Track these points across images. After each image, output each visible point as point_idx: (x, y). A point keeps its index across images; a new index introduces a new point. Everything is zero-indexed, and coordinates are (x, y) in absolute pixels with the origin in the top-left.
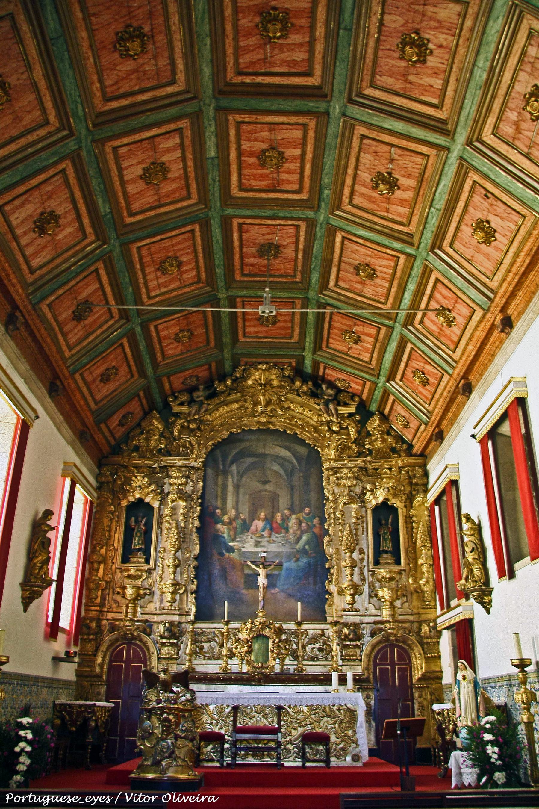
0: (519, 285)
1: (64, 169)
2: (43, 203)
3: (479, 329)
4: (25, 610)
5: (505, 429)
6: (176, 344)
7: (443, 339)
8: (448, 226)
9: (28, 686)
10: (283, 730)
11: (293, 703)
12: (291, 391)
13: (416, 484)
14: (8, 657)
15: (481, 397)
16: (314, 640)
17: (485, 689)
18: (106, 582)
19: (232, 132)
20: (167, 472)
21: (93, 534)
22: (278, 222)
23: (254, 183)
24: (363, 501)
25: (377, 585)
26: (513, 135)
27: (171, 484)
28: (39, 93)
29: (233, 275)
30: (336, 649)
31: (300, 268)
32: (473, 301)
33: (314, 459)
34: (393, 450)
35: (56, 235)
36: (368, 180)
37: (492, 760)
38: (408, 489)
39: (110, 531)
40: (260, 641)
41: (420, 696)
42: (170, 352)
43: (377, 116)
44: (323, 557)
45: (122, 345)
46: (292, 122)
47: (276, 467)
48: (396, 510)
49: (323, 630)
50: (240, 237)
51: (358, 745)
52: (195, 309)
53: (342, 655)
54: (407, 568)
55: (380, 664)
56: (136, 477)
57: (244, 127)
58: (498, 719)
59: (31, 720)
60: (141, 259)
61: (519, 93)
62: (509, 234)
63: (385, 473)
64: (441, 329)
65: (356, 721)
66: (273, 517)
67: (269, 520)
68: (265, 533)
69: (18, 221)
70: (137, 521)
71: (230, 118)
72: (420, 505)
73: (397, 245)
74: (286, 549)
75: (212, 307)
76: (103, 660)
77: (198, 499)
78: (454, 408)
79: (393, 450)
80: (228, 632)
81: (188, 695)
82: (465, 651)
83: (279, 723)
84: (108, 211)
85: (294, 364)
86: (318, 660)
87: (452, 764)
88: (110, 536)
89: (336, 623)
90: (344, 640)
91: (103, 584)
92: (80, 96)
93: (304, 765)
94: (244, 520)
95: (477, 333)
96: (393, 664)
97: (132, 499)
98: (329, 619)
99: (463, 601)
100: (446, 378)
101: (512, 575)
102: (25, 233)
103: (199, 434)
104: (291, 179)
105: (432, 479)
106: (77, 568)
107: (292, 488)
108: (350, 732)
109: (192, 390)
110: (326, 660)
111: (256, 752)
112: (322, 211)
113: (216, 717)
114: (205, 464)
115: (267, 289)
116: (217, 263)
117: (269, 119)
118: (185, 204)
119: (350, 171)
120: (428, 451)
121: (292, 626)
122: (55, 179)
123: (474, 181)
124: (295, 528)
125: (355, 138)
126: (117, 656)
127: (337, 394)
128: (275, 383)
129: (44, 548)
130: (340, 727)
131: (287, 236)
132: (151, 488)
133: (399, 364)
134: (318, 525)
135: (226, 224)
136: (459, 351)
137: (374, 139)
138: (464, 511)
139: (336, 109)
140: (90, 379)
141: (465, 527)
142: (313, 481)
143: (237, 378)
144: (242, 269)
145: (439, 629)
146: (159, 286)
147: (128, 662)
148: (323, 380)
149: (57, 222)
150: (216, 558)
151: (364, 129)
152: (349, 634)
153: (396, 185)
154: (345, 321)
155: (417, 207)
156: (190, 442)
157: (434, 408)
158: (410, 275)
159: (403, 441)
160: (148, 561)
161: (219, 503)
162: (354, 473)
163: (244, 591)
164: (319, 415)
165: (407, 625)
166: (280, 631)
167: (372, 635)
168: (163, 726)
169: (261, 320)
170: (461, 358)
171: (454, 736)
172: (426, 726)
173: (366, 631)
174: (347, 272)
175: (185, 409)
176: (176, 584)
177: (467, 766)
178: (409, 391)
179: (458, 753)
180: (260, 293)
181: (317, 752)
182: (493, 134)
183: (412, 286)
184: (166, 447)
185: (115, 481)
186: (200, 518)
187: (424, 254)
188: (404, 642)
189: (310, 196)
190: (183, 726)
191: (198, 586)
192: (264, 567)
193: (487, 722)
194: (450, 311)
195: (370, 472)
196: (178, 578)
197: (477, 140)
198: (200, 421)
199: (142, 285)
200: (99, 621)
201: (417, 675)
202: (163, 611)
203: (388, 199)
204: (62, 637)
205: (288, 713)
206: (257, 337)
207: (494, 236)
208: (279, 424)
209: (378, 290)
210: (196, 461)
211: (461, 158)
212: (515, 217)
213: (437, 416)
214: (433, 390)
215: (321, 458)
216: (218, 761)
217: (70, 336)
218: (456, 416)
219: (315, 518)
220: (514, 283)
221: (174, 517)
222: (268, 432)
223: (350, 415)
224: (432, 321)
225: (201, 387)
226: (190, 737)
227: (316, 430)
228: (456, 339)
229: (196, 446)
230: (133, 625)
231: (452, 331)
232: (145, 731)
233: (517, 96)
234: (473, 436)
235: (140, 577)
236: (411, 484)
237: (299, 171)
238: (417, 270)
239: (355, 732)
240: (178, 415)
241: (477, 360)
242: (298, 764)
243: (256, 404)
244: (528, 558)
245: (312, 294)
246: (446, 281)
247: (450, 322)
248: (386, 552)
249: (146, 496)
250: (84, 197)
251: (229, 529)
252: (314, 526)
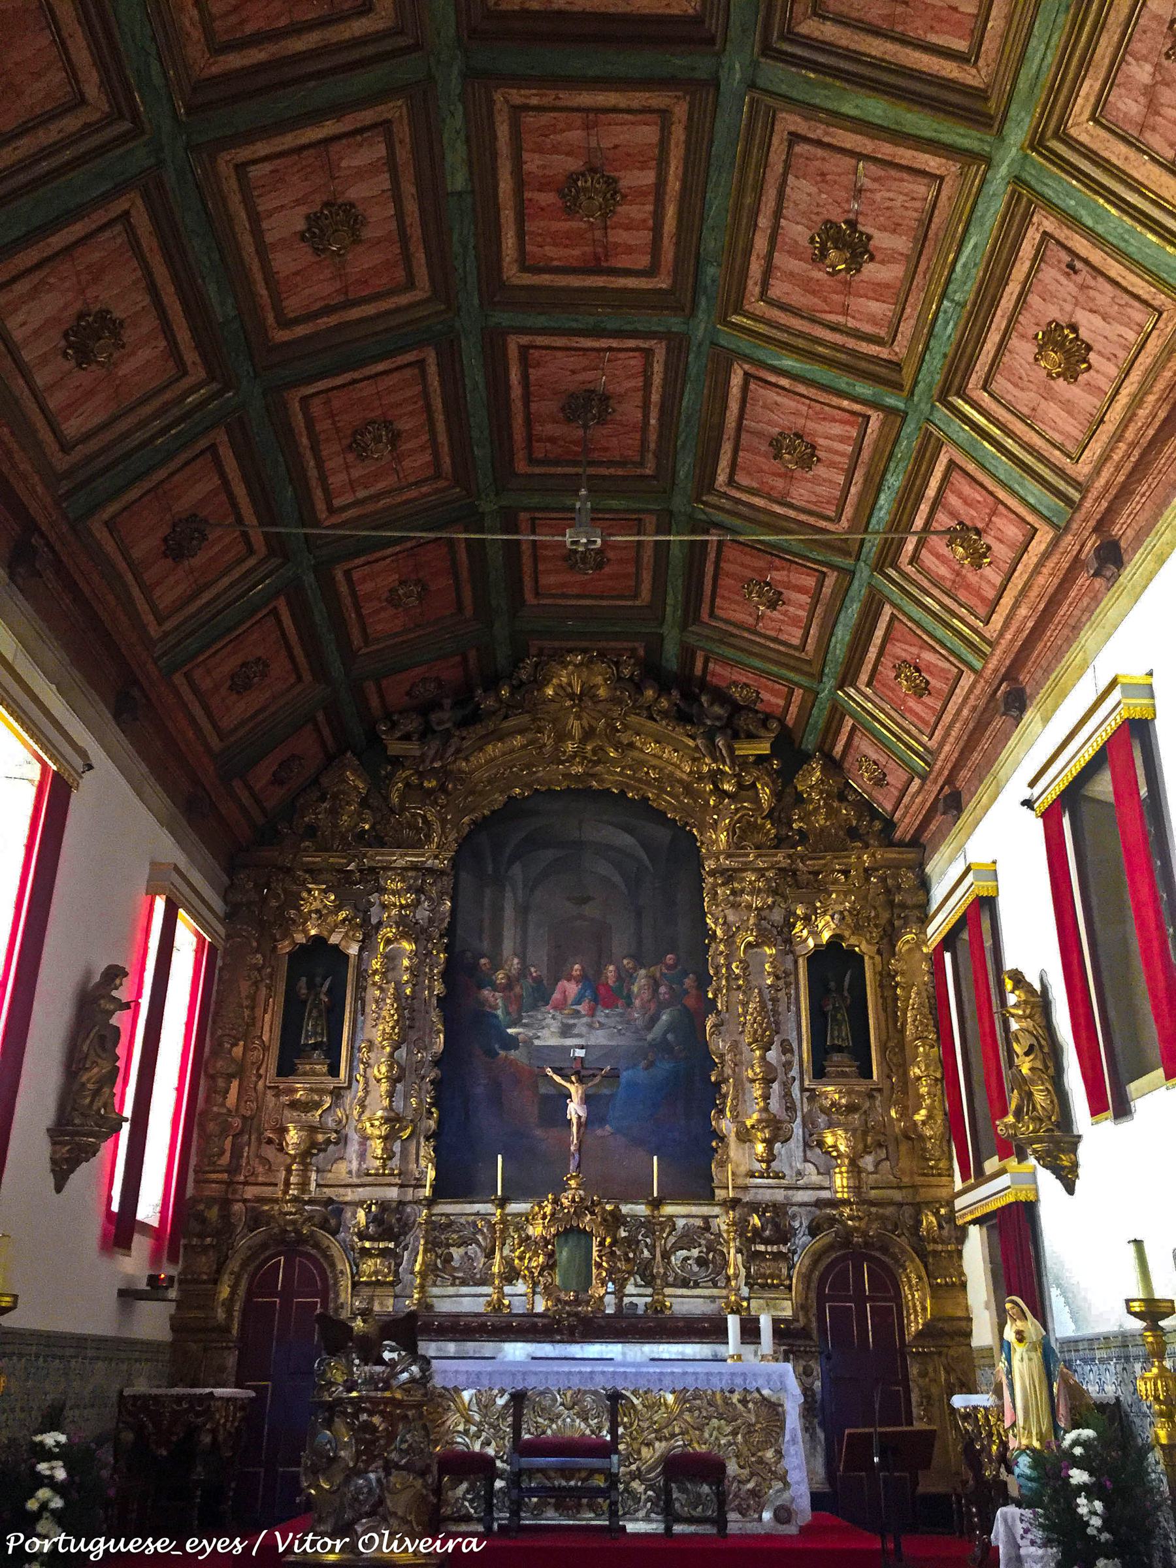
0: (1140, 470)
1: (127, 213)
2: (83, 292)
3: (1045, 571)
4: (59, 1189)
5: (1103, 787)
6: (392, 611)
7: (962, 595)
8: (980, 341)
9: (61, 1358)
10: (621, 1447)
11: (643, 1385)
12: (636, 709)
13: (903, 906)
14: (16, 1297)
15: (1046, 720)
16: (687, 1239)
17: (1069, 1364)
18: (244, 1117)
19: (503, 131)
20: (377, 880)
21: (216, 1014)
22: (604, 343)
23: (550, 251)
24: (789, 941)
25: (822, 1120)
26: (1139, 119)
27: (384, 907)
28: (59, 30)
29: (512, 460)
30: (735, 1258)
31: (653, 446)
32: (1034, 510)
33: (683, 853)
34: (853, 833)
35: (115, 365)
36: (804, 241)
37: (1090, 1531)
38: (886, 915)
39: (252, 1008)
40: (572, 1240)
41: (923, 1374)
42: (379, 627)
43: (826, 86)
44: (705, 1059)
45: (275, 612)
46: (635, 104)
47: (604, 868)
48: (860, 958)
49: (706, 1219)
50: (525, 377)
51: (787, 1485)
52: (432, 535)
53: (748, 1276)
54: (886, 1086)
55: (831, 1298)
56: (309, 891)
57: (529, 119)
58: (1100, 1437)
59: (63, 1438)
60: (310, 423)
61: (1157, 18)
62: (1122, 354)
63: (836, 881)
64: (958, 574)
65: (783, 1428)
66: (599, 972)
68: (582, 1008)
69: (28, 330)
70: (311, 986)
71: (498, 96)
72: (910, 950)
73: (864, 389)
74: (624, 1042)
75: (466, 531)
76: (233, 1293)
77: (442, 936)
78: (985, 744)
79: (853, 833)
80: (503, 1221)
81: (415, 1369)
82: (1021, 1269)
83: (613, 1431)
84: (233, 313)
85: (641, 652)
86: (697, 1285)
87: (999, 1527)
88: (254, 1018)
89: (734, 1203)
90: (752, 1241)
91: (237, 1122)
92: (154, 38)
93: (668, 1529)
94: (538, 980)
95: (1041, 580)
96: (861, 1300)
97: (300, 938)
98: (720, 1194)
99: (1012, 1162)
100: (967, 680)
101: (1123, 1111)
102: (44, 360)
103: (442, 799)
104: (632, 242)
105: (938, 892)
106: (180, 1090)
107: (639, 915)
108: (770, 1454)
109: (426, 709)
110: (715, 1286)
111: (564, 1499)
112: (701, 315)
113: (477, 1418)
114: (455, 862)
115: (583, 492)
116: (475, 434)
117: (586, 99)
118: (403, 300)
119: (764, 222)
120: (927, 834)
121: (642, 1209)
122: (107, 234)
123: (1045, 233)
124: (646, 996)
125: (775, 141)
126: (262, 1283)
127: (731, 717)
128: (602, 692)
129: (104, 1049)
130: (745, 1441)
131: (626, 372)
132: (342, 915)
133: (865, 651)
134: (693, 992)
135: (493, 345)
136: (998, 620)
137: (819, 143)
138: (1009, 964)
139: (735, 72)
140: (207, 684)
141: (1012, 999)
143: (522, 684)
144: (529, 448)
145: (960, 1222)
146: (352, 485)
147: (287, 1294)
148: (703, 685)
149: (116, 334)
151: (798, 119)
152: (763, 1228)
153: (867, 251)
154: (747, 560)
155: (911, 300)
156: (424, 817)
157: (941, 744)
158: (891, 454)
159: (874, 814)
160: (334, 1071)
161: (486, 945)
162: (768, 880)
163: (538, 1132)
164: (694, 760)
165: (889, 1211)
166: (615, 1220)
167: (813, 1231)
168: (359, 1441)
169: (571, 558)
170: (1001, 635)
171: (1002, 1470)
172: (937, 1444)
173: (800, 1223)
174: (755, 451)
175: (413, 748)
176: (393, 1120)
177: (1033, 1543)
178: (887, 707)
179: (1011, 1510)
180: (569, 503)
181: (698, 1500)
182: (1093, 118)
183: (895, 481)
184: (372, 827)
185: (264, 900)
186: (445, 976)
187: (925, 407)
188: (885, 1249)
189: (675, 282)
190: (403, 1441)
191: (440, 1123)
192: (581, 1081)
193: (1076, 1443)
194: (978, 532)
195: (804, 878)
196: (399, 1104)
197: (1056, 135)
198: (445, 774)
199: (314, 483)
200: (225, 1204)
201: (915, 1325)
202: (367, 1178)
203: (847, 284)
204: (141, 1245)
205: (633, 1406)
206: (565, 596)
207: (1085, 361)
208: (612, 778)
209: (821, 490)
210: (436, 857)
211: (1018, 180)
212: (1138, 314)
213: (946, 760)
214: (938, 705)
215: (698, 850)
216: (479, 1520)
217: (157, 593)
218: (990, 760)
219: (686, 975)
220: (1129, 466)
221: (390, 975)
222: (589, 793)
223: (760, 759)
224: (938, 556)
225: (447, 702)
226: (419, 1465)
227: (688, 790)
228: (990, 594)
229: (437, 826)
230: (300, 1211)
231: (982, 577)
232: (319, 1453)
233: (1154, 25)
234: (1028, 803)
235: (318, 1105)
236: (891, 904)
237: (651, 222)
238: (908, 444)
239: (779, 1453)
240: (397, 762)
241: (1040, 639)
242: (653, 1527)
243: (562, 736)
244: (1160, 1072)
245: (678, 503)
246: (971, 467)
247: (978, 557)
248: (840, 1049)
249: (332, 932)
250: (176, 279)
251: (504, 999)
252: (686, 992)
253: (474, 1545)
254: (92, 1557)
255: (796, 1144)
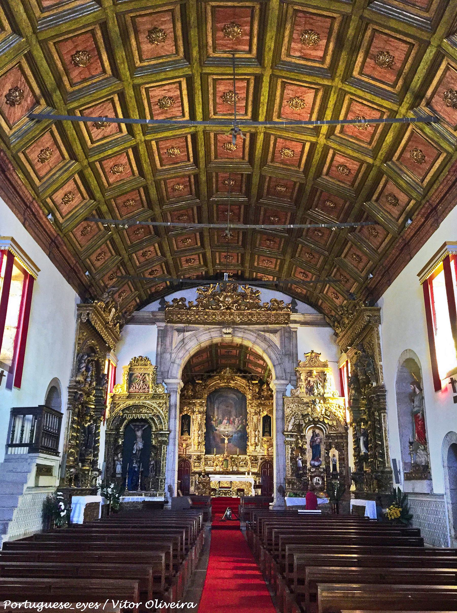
16: (243, 461)
30: (249, 463)
33: (244, 398)
44: (246, 433)
47: (231, 402)
67: (229, 420)
74: (234, 430)
89: (249, 456)
98: (248, 454)
121: (236, 456)
142: (243, 406)
150: (211, 433)
167: (261, 459)
223: (256, 384)
253: (192, 605)
254: (38, 610)
255: (259, 446)
